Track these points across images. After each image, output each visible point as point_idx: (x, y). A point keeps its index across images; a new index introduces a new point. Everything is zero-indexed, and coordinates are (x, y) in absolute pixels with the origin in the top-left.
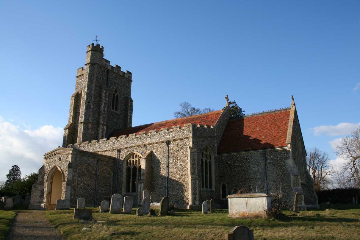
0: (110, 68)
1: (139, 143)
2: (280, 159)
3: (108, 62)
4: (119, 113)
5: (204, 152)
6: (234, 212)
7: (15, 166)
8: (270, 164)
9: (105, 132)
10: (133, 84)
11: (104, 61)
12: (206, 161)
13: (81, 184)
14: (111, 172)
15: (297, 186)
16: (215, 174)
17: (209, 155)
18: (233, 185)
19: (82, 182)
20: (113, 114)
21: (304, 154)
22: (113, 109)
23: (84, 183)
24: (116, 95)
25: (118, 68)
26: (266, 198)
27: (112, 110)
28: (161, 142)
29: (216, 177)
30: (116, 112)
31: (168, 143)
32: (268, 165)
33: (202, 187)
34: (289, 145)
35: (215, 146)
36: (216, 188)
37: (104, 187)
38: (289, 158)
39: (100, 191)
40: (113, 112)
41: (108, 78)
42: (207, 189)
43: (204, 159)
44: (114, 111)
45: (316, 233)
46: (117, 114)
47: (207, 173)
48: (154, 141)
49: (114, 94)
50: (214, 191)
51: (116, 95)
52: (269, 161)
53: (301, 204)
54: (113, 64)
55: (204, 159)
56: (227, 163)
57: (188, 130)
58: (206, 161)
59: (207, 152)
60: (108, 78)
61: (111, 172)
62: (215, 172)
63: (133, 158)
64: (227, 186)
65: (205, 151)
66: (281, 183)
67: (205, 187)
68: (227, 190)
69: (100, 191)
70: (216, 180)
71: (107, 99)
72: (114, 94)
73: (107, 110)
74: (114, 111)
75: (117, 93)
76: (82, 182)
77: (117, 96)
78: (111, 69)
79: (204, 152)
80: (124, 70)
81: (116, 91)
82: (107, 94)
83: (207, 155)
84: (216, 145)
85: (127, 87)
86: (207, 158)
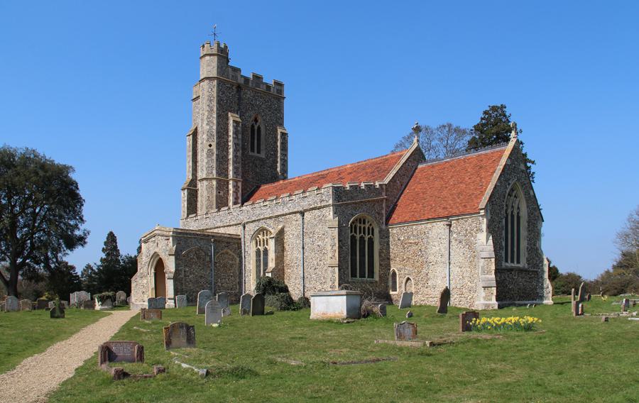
0: (241, 81)
1: (268, 213)
2: (470, 233)
3: (236, 70)
4: (264, 157)
5: (358, 225)
6: (316, 312)
7: (494, 109)
8: (456, 240)
9: (240, 191)
10: (286, 102)
11: (230, 69)
12: (362, 238)
13: (190, 276)
14: (236, 257)
15: (487, 274)
16: (380, 256)
17: (369, 228)
18: (406, 272)
19: (190, 274)
20: (253, 159)
21: (538, 217)
22: (252, 150)
23: (194, 274)
24: (256, 128)
25: (258, 78)
26: (345, 297)
27: (250, 153)
28: (295, 213)
29: (381, 260)
30: (258, 155)
31: (302, 213)
32: (453, 241)
33: (352, 276)
34: (483, 211)
35: (382, 214)
36: (380, 277)
37: (225, 279)
38: (481, 230)
39: (220, 285)
40: (252, 156)
41: (240, 99)
42: (371, 279)
43: (358, 236)
44: (255, 154)
45: (586, 350)
46: (261, 159)
47: (364, 256)
48: (286, 211)
49: (253, 126)
50: (376, 282)
51: (256, 128)
52: (454, 235)
53: (491, 300)
54: (247, 73)
55: (358, 236)
56: (399, 240)
57: (327, 192)
58: (362, 238)
59: (364, 223)
60: (240, 99)
61: (236, 257)
62: (380, 253)
63: (264, 236)
64: (397, 274)
65: (360, 223)
66: (468, 269)
67: (509, 261)
68: (398, 279)
69: (220, 285)
70: (380, 265)
71: (240, 136)
72: (253, 126)
73: (240, 155)
74: (515, 265)
75: (258, 124)
76: (190, 274)
77: (259, 128)
78: (245, 81)
79: (358, 225)
80: (269, 79)
81: (256, 120)
82: (239, 129)
83: (364, 228)
84: (384, 212)
85: (276, 110)
86: (364, 233)
